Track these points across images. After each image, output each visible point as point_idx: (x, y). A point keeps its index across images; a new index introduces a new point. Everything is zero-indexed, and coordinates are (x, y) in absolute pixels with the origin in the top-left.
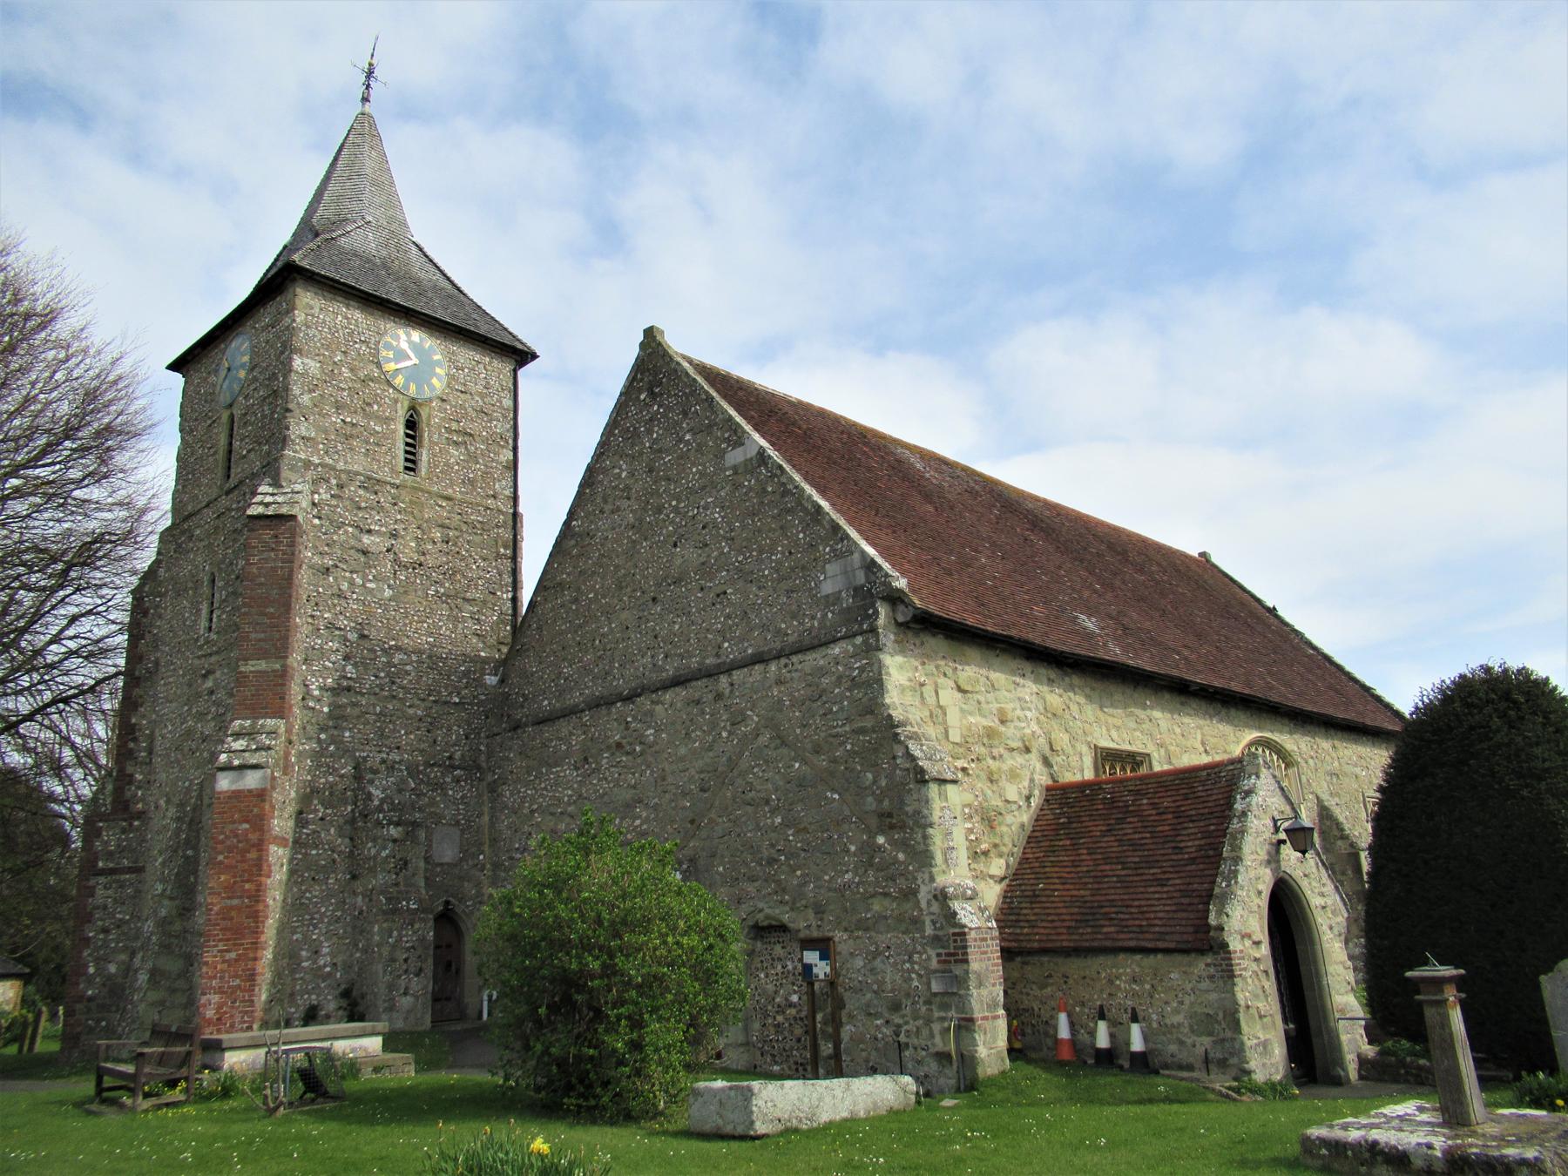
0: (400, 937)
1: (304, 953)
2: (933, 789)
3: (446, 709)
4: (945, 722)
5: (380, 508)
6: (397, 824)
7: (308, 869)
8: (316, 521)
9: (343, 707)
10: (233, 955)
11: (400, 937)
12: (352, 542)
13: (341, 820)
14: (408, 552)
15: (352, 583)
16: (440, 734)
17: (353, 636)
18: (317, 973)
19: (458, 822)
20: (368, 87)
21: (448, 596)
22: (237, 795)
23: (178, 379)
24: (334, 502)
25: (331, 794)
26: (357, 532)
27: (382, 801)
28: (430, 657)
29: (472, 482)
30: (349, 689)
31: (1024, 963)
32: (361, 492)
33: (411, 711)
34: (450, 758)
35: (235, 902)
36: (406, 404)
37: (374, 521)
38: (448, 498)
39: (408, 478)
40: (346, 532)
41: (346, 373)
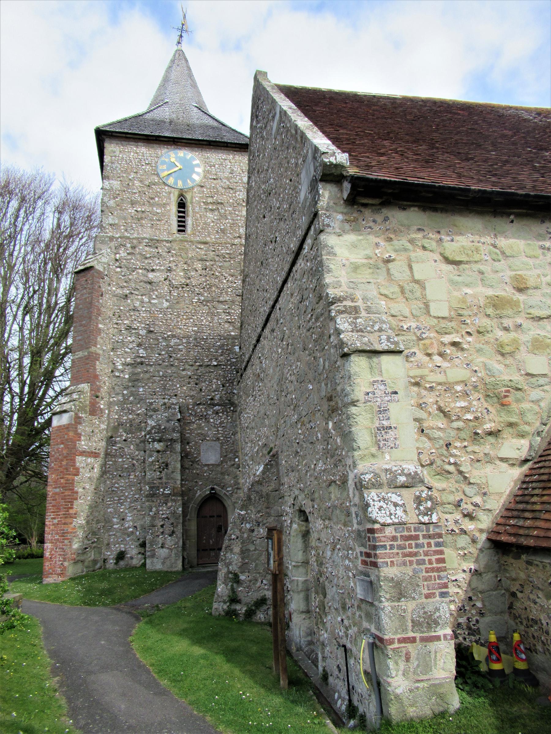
0: (158, 511)
1: (115, 520)
2: (358, 365)
3: (208, 369)
4: (424, 296)
5: (159, 256)
6: (159, 441)
7: (117, 470)
8: (119, 270)
9: (138, 374)
11: (158, 511)
12: (142, 278)
13: (138, 441)
14: (178, 277)
15: (142, 302)
16: (203, 385)
17: (143, 332)
18: (124, 532)
19: (218, 439)
20: (181, 36)
21: (208, 301)
24: (129, 257)
25: (131, 425)
26: (145, 272)
28: (195, 339)
29: (223, 231)
30: (142, 363)
31: (529, 563)
32: (147, 249)
33: (184, 373)
34: (212, 399)
36: (177, 193)
37: (155, 264)
38: (205, 243)
39: (180, 236)
40: (138, 273)
41: (137, 183)
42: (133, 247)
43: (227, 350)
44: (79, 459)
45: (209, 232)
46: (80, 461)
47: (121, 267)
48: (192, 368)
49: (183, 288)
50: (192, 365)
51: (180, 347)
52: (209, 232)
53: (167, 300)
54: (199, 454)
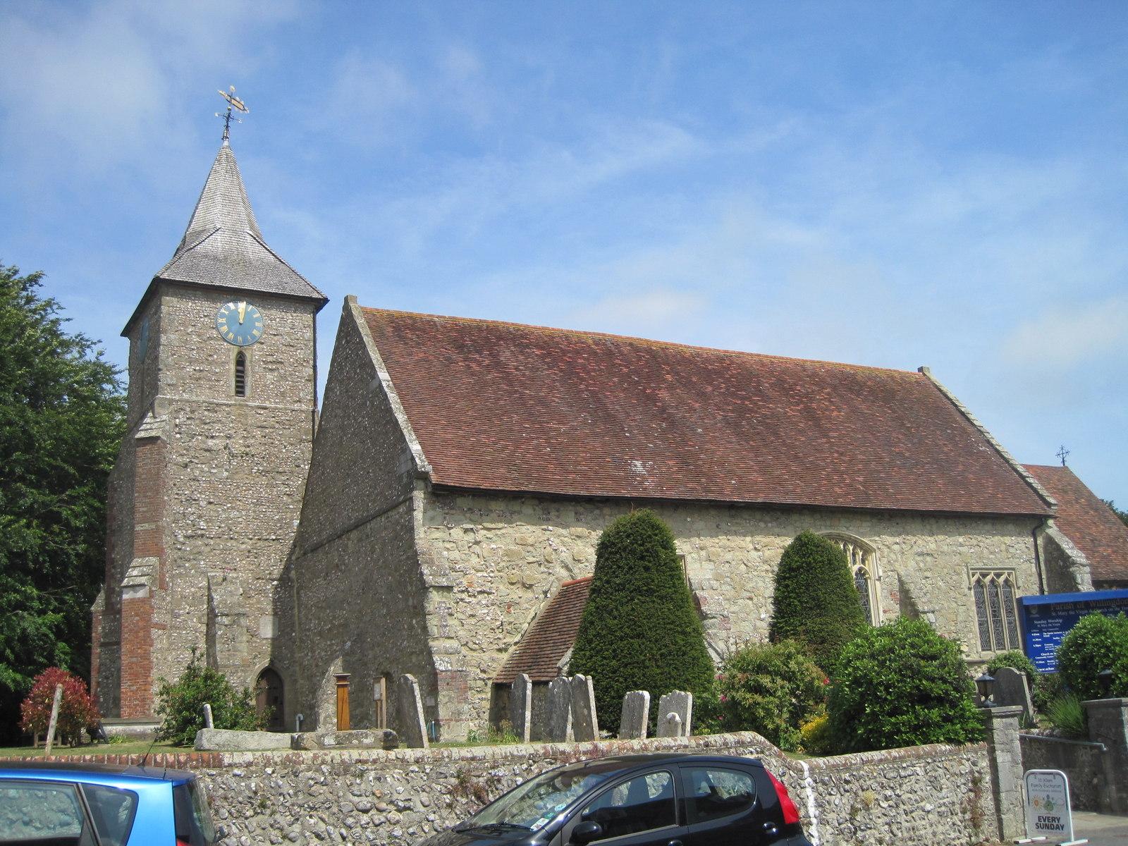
8: (178, 436)
10: (135, 688)
14: (237, 446)
22: (132, 601)
23: (126, 341)
24: (189, 422)
25: (193, 599)
26: (204, 438)
27: (220, 602)
29: (283, 394)
30: (202, 536)
32: (206, 413)
33: (244, 546)
35: (134, 659)
40: (197, 439)
42: (192, 412)
43: (285, 523)
44: (154, 631)
45: (268, 395)
46: (155, 633)
47: (180, 433)
48: (251, 542)
49: (242, 457)
50: (251, 539)
51: (240, 520)
52: (268, 395)
53: (226, 470)
54: (258, 628)
